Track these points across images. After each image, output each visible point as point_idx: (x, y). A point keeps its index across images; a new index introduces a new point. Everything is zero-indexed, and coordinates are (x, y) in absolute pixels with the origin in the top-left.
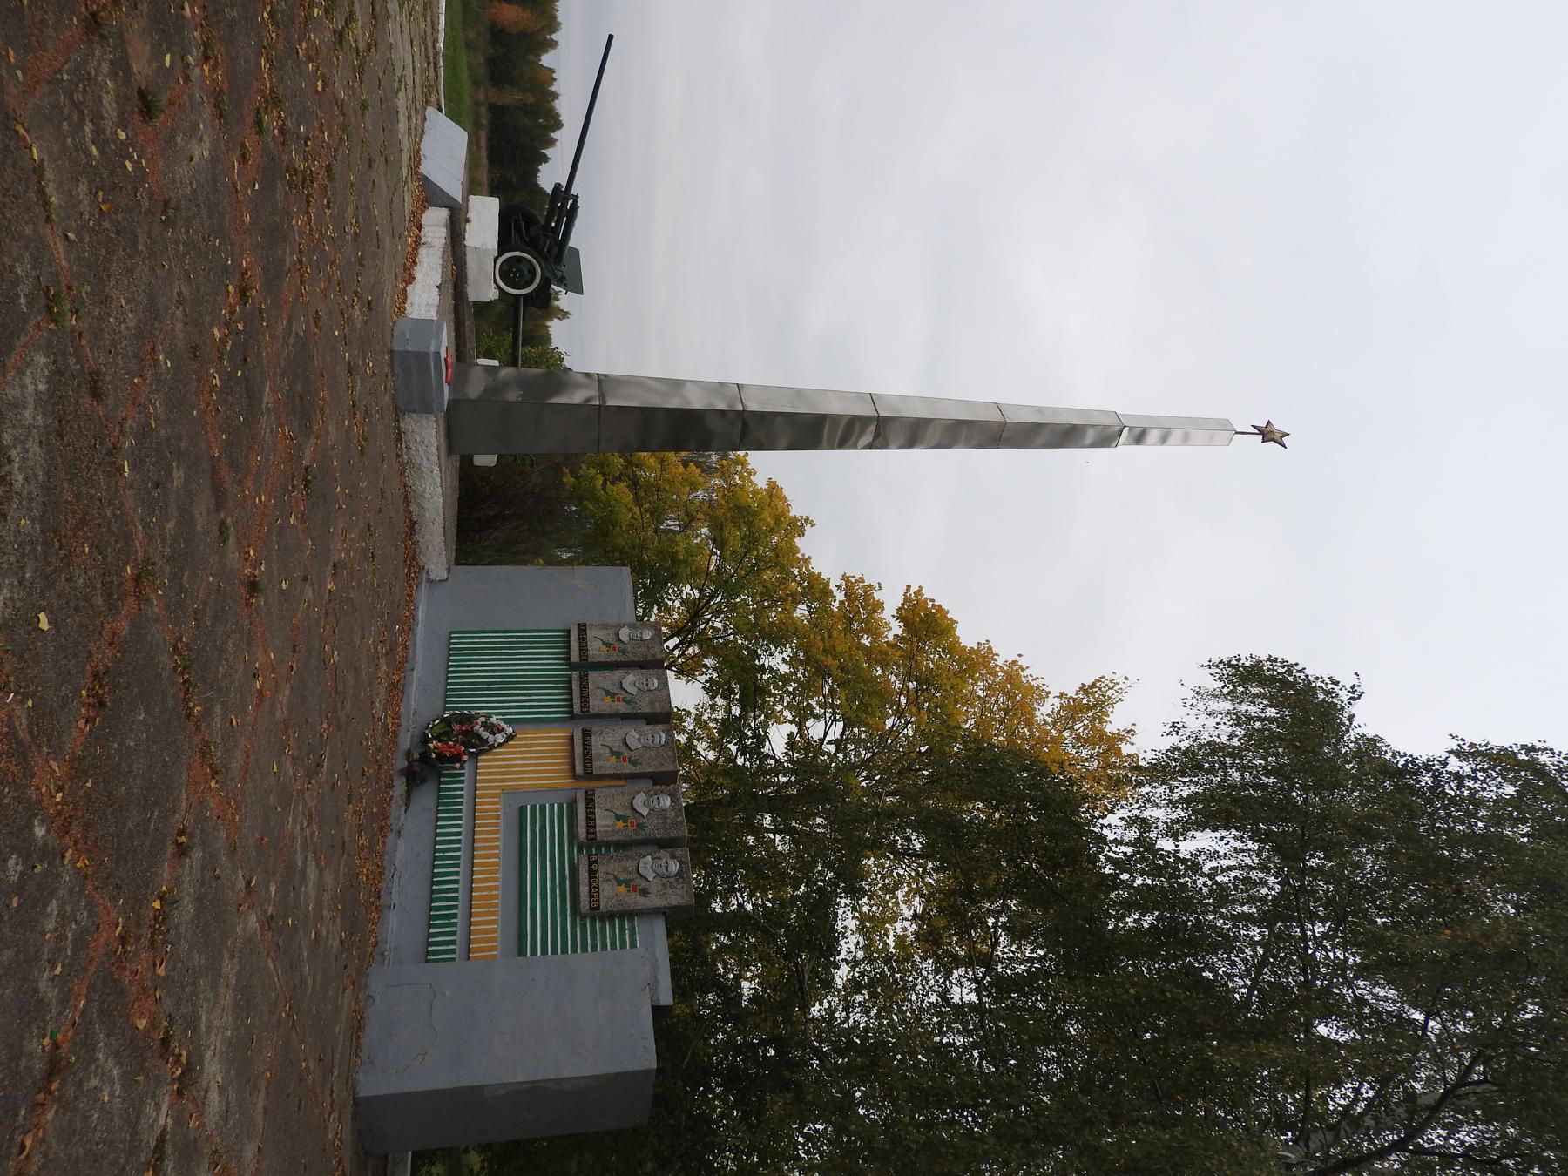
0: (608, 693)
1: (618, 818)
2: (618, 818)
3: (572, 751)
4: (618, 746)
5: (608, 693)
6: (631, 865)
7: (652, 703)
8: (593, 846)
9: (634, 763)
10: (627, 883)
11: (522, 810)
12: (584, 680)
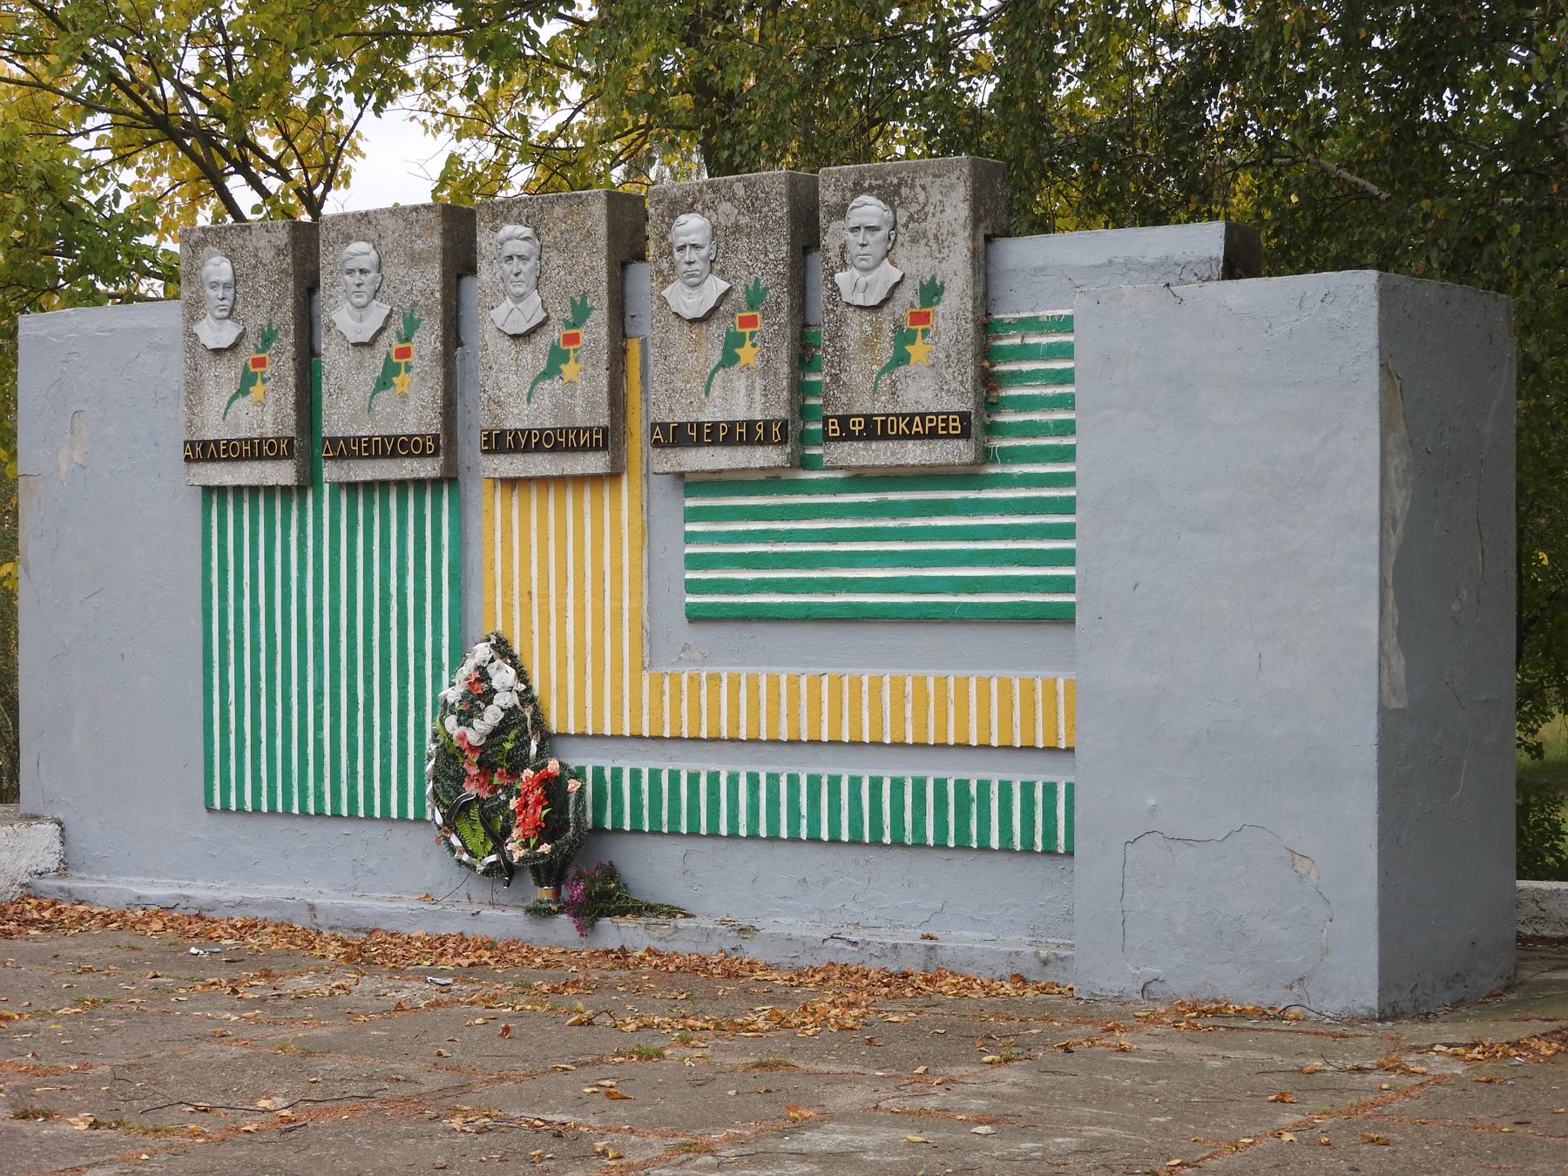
0: (384, 383)
1: (729, 359)
2: (729, 359)
3: (543, 481)
4: (534, 357)
5: (384, 383)
6: (856, 328)
7: (415, 259)
8: (798, 429)
9: (581, 312)
10: (903, 338)
11: (697, 617)
12: (347, 449)
